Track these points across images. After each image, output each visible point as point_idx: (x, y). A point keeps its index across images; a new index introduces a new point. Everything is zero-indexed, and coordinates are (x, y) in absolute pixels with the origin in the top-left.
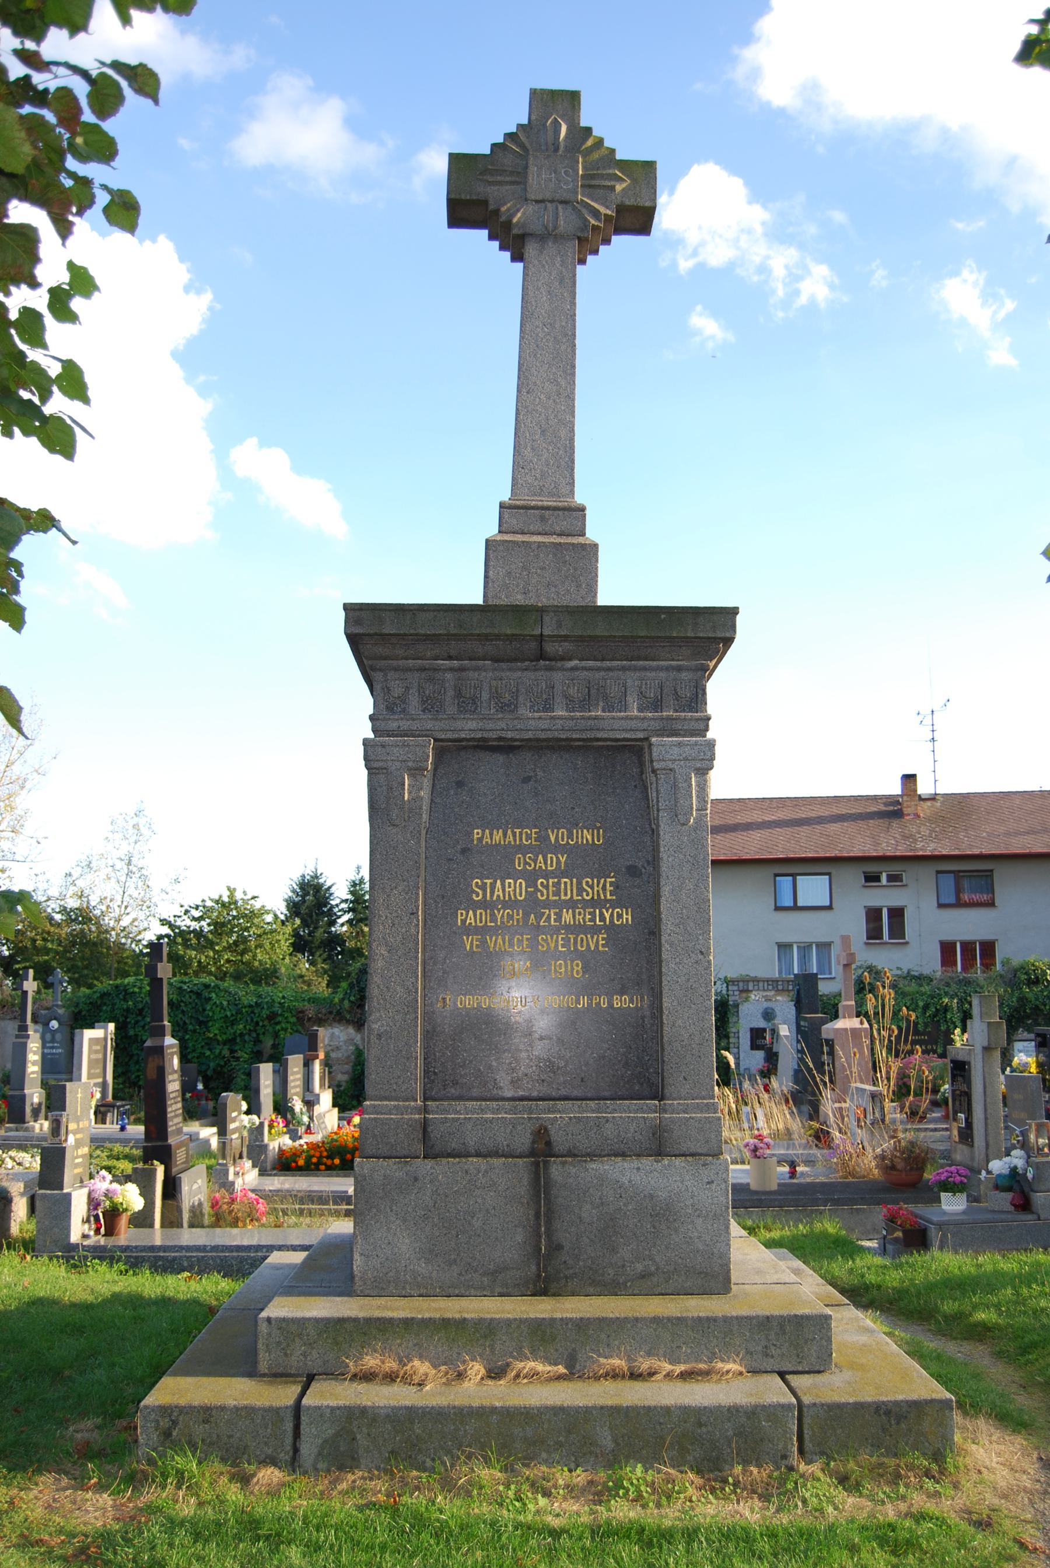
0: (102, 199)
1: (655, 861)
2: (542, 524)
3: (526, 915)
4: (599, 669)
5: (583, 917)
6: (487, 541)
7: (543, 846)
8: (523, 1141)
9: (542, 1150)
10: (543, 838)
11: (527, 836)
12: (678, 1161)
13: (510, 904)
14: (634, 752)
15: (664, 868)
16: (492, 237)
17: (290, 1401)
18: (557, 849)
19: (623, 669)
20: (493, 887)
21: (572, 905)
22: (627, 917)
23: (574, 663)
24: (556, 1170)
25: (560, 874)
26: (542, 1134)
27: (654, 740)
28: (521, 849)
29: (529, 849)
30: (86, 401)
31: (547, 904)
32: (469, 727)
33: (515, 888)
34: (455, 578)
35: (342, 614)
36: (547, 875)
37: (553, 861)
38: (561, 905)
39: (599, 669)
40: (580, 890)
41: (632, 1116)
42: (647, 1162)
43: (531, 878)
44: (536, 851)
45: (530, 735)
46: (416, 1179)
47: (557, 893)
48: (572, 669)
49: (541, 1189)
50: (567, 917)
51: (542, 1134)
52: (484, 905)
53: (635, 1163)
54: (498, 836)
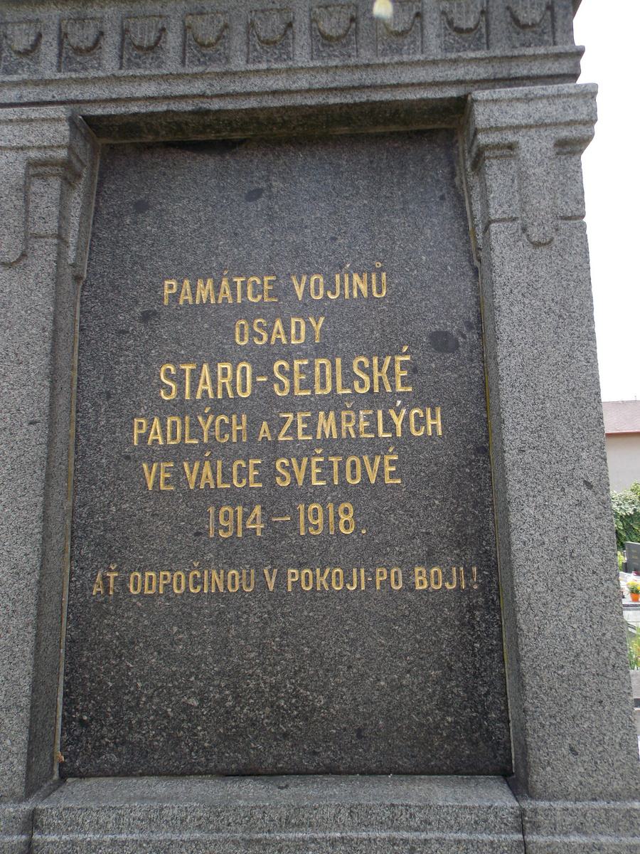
3: (254, 425)
5: (357, 424)
10: (282, 292)
11: (251, 288)
18: (307, 308)
21: (334, 403)
22: (434, 423)
28: (245, 310)
29: (260, 309)
31: (291, 404)
32: (141, 92)
36: (289, 354)
37: (299, 331)
40: (349, 378)
43: (262, 359)
50: (326, 425)
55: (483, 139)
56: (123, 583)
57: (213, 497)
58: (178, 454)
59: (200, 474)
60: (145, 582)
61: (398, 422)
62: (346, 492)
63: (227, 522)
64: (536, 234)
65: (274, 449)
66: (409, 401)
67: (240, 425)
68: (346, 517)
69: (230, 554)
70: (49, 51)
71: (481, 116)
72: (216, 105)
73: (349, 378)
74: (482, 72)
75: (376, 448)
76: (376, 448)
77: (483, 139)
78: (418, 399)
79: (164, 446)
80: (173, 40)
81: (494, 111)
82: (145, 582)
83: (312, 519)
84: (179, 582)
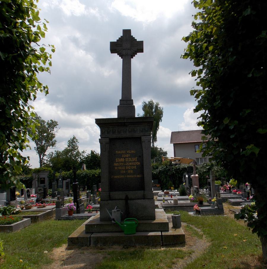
0: (28, 106)
1: (143, 155)
2: (126, 103)
3: (124, 164)
4: (133, 127)
5: (132, 164)
6: (118, 106)
7: (126, 153)
8: (124, 197)
9: (127, 199)
10: (126, 152)
11: (124, 152)
12: (147, 200)
13: (122, 162)
14: (139, 139)
15: (144, 156)
16: (119, 38)
17: (89, 236)
18: (128, 154)
19: (137, 126)
20: (119, 159)
21: (131, 162)
22: (139, 163)
23: (129, 126)
24: (129, 201)
25: (129, 157)
26: (127, 196)
27: (142, 137)
28: (123, 154)
29: (124, 154)
30: (22, 152)
31: (127, 162)
32: (114, 136)
33: (122, 160)
34: (114, 114)
35: (95, 120)
36: (127, 158)
37: (128, 155)
38: (129, 162)
39: (133, 127)
40: (132, 160)
41: (140, 193)
42: (142, 200)
43: (125, 158)
44: (125, 154)
45: (124, 137)
46: (109, 203)
47: (129, 160)
48: (129, 127)
49: (127, 203)
50: (130, 164)
51: (127, 196)
52: (118, 162)
53: (140, 200)
54: (120, 152)
55: (142, 141)
56: (114, 177)
57: (121, 170)
58: (118, 166)
59: (120, 168)
60: (116, 177)
61: (136, 163)
62: (132, 169)
63: (122, 172)
64: (146, 148)
65: (126, 166)
66: (137, 162)
67: (123, 164)
68: (132, 172)
69: (123, 174)
70: (106, 132)
71: (142, 139)
72: (120, 137)
73: (132, 160)
74: (142, 135)
75: (134, 165)
76: (134, 165)
77: (142, 141)
78: (138, 161)
79: (31, 116)
80: (117, 131)
81: (143, 138)
82: (116, 177)
83: (129, 172)
84: (118, 177)
